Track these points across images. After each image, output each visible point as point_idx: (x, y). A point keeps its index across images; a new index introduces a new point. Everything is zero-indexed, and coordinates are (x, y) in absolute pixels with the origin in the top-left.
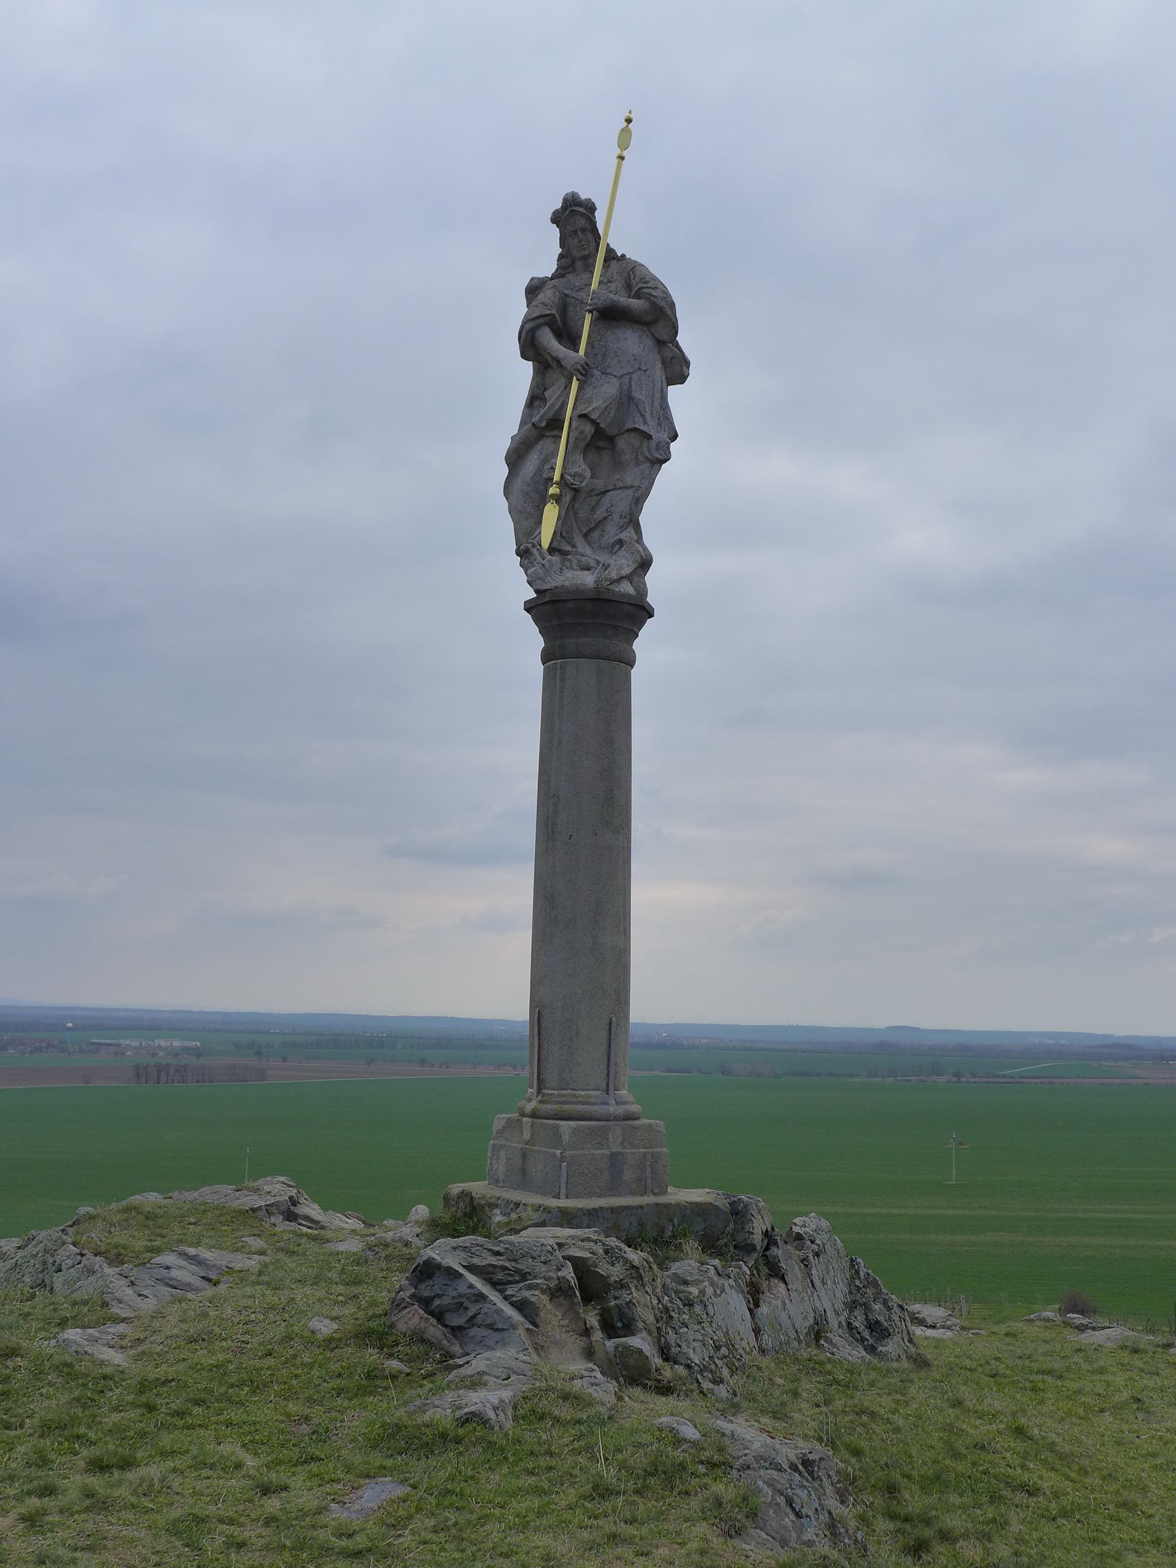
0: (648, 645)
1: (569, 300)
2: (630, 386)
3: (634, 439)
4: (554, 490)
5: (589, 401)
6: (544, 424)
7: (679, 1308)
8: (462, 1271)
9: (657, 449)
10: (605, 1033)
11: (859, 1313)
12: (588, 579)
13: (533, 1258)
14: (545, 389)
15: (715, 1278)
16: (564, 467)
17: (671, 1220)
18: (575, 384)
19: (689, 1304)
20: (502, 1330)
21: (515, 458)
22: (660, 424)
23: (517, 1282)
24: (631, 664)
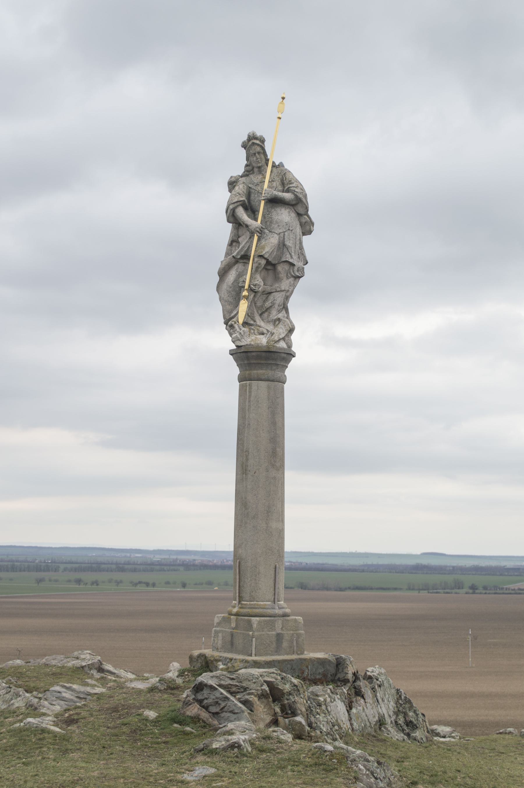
0: (292, 370)
1: (251, 190)
2: (284, 239)
3: (286, 267)
4: (245, 293)
5: (263, 248)
6: (239, 257)
7: (315, 707)
8: (217, 687)
9: (298, 271)
10: (273, 572)
11: (401, 717)
12: (263, 340)
13: (249, 681)
14: (239, 237)
15: (331, 694)
16: (250, 281)
17: (307, 667)
18: (256, 238)
19: (320, 705)
20: (237, 713)
21: (223, 273)
22: (299, 258)
23: (242, 692)
24: (284, 383)
